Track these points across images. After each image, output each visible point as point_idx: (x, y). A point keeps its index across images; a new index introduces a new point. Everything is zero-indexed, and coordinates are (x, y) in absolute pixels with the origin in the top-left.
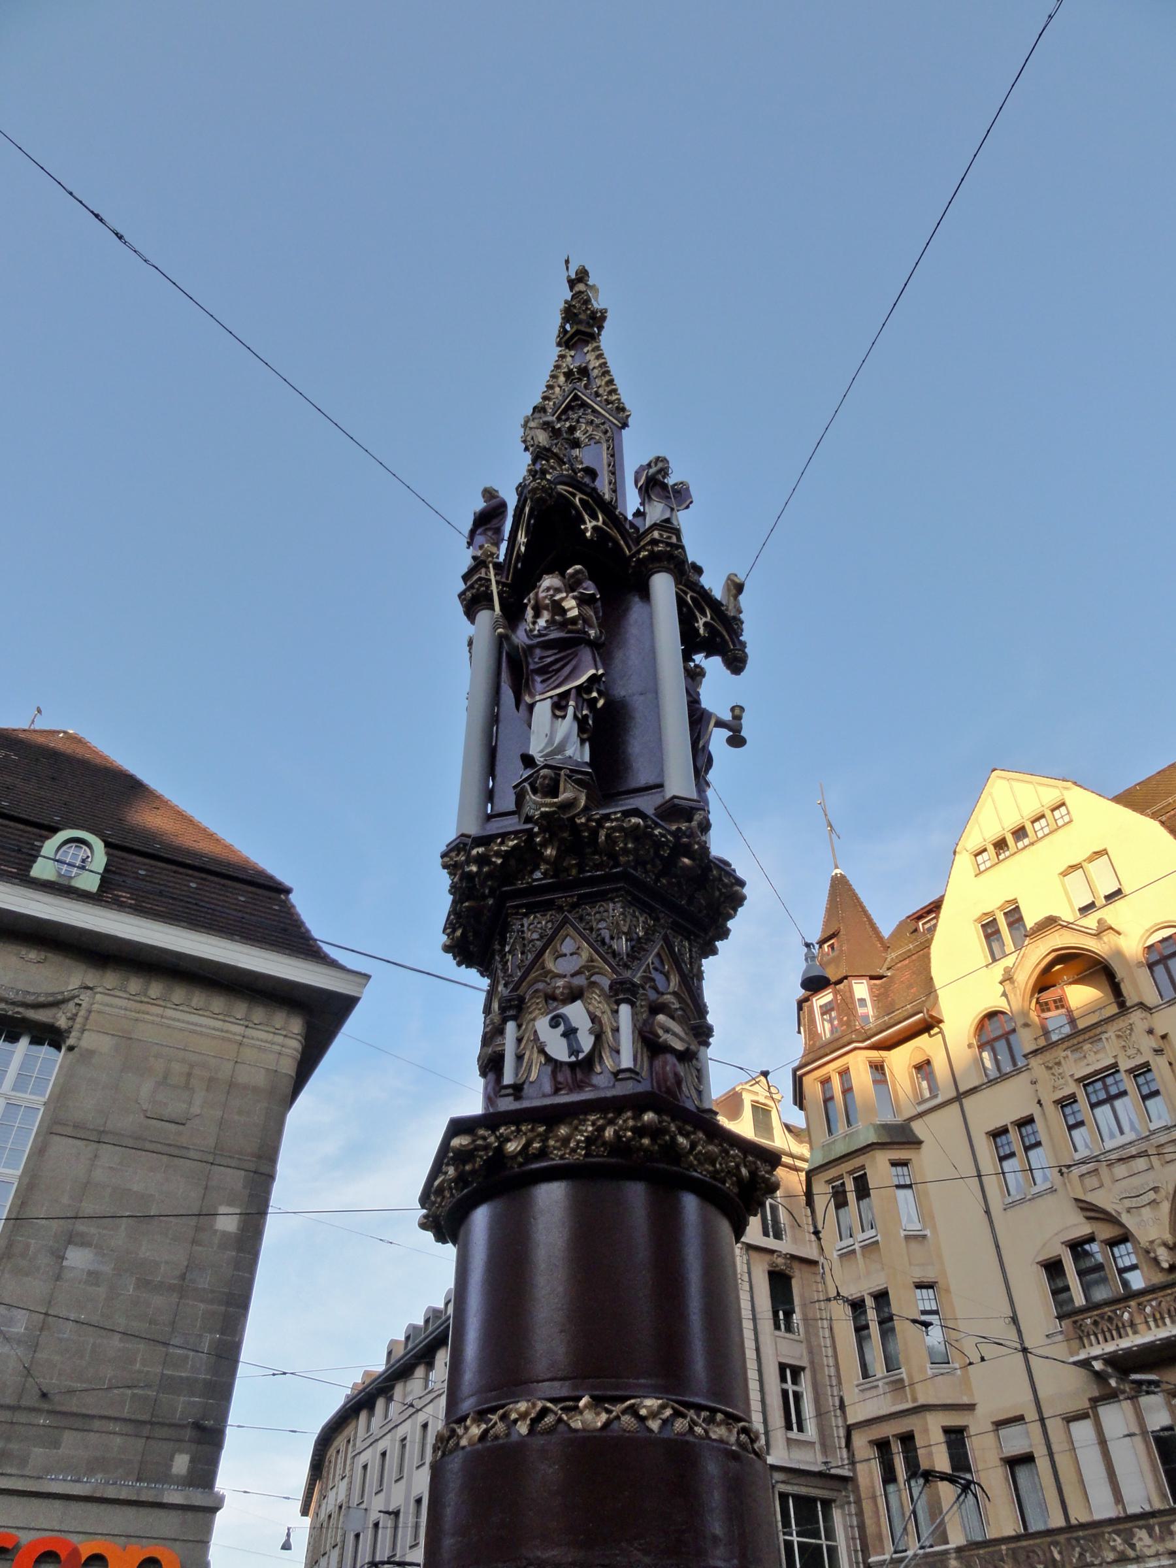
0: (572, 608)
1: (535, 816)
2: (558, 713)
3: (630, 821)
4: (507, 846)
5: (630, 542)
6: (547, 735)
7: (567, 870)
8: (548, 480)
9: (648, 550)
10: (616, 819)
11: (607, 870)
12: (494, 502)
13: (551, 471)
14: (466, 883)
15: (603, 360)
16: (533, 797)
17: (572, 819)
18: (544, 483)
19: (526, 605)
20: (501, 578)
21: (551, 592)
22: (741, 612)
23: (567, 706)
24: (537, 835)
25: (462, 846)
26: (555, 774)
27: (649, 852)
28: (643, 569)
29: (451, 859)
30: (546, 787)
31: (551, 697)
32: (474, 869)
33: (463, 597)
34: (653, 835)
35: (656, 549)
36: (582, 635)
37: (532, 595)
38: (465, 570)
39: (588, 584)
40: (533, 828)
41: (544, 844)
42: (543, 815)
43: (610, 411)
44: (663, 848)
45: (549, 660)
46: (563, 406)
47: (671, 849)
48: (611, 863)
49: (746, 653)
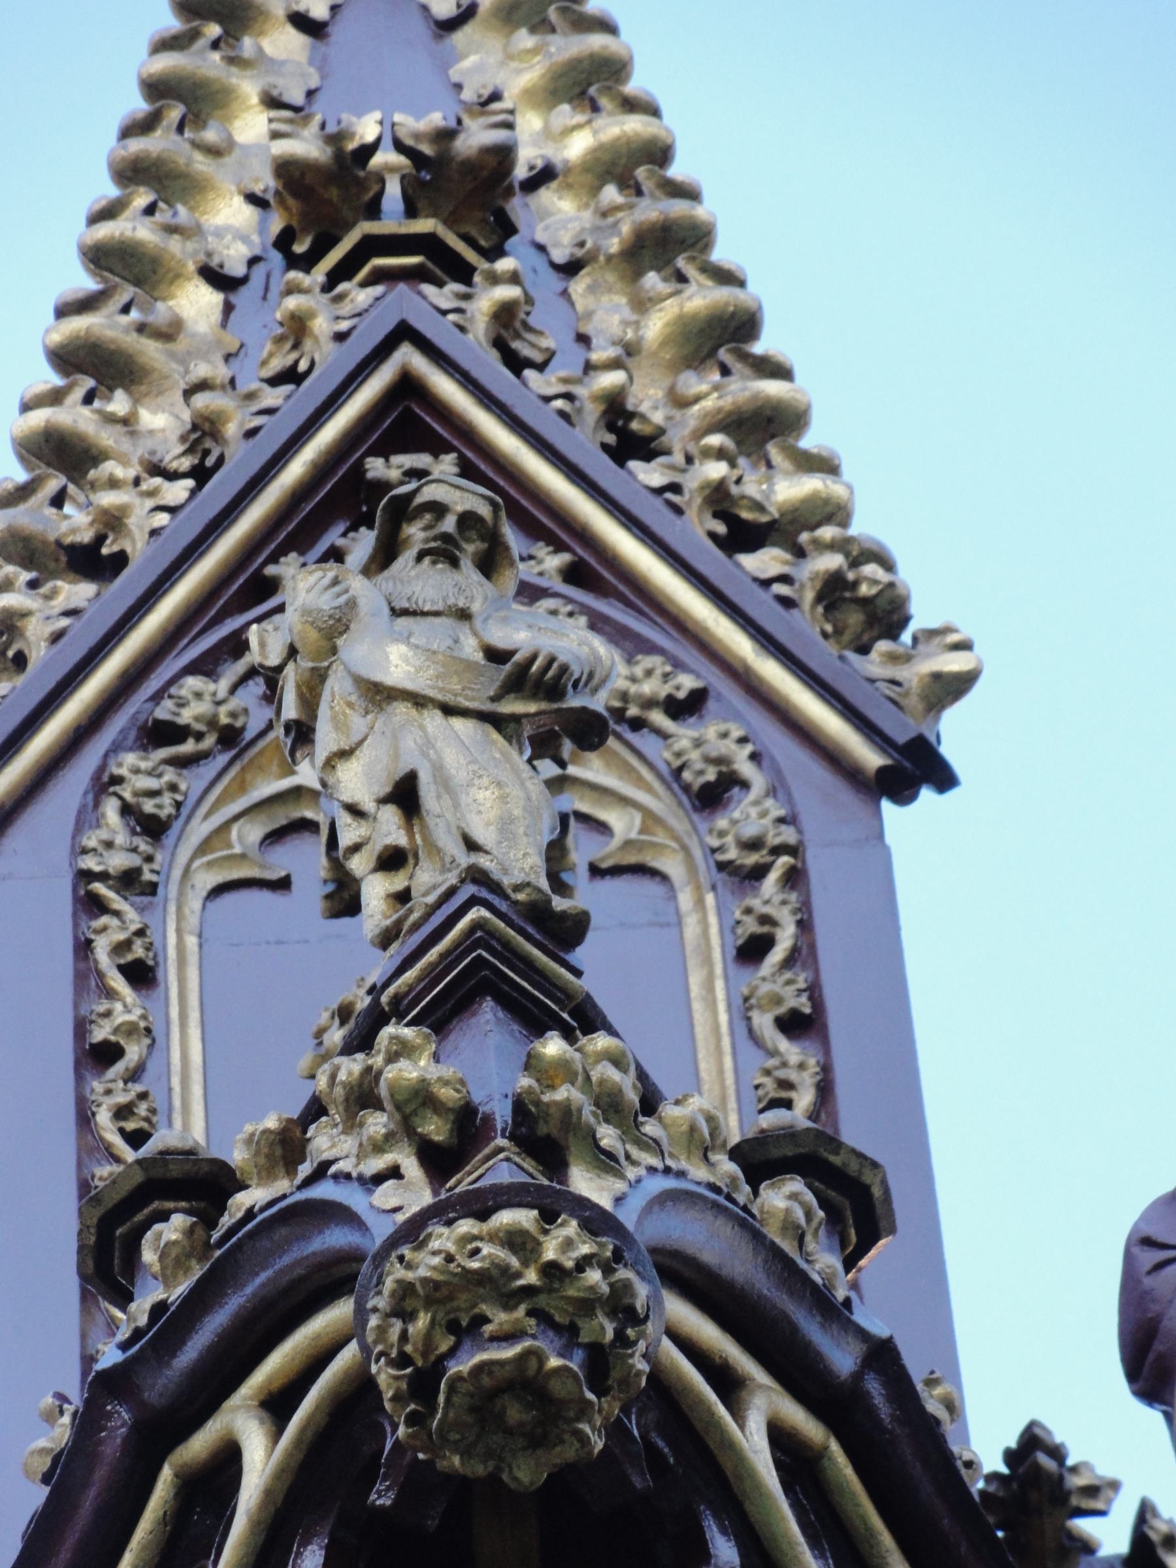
13: (608, 1136)
15: (634, 125)
43: (762, 607)
46: (296, 469)
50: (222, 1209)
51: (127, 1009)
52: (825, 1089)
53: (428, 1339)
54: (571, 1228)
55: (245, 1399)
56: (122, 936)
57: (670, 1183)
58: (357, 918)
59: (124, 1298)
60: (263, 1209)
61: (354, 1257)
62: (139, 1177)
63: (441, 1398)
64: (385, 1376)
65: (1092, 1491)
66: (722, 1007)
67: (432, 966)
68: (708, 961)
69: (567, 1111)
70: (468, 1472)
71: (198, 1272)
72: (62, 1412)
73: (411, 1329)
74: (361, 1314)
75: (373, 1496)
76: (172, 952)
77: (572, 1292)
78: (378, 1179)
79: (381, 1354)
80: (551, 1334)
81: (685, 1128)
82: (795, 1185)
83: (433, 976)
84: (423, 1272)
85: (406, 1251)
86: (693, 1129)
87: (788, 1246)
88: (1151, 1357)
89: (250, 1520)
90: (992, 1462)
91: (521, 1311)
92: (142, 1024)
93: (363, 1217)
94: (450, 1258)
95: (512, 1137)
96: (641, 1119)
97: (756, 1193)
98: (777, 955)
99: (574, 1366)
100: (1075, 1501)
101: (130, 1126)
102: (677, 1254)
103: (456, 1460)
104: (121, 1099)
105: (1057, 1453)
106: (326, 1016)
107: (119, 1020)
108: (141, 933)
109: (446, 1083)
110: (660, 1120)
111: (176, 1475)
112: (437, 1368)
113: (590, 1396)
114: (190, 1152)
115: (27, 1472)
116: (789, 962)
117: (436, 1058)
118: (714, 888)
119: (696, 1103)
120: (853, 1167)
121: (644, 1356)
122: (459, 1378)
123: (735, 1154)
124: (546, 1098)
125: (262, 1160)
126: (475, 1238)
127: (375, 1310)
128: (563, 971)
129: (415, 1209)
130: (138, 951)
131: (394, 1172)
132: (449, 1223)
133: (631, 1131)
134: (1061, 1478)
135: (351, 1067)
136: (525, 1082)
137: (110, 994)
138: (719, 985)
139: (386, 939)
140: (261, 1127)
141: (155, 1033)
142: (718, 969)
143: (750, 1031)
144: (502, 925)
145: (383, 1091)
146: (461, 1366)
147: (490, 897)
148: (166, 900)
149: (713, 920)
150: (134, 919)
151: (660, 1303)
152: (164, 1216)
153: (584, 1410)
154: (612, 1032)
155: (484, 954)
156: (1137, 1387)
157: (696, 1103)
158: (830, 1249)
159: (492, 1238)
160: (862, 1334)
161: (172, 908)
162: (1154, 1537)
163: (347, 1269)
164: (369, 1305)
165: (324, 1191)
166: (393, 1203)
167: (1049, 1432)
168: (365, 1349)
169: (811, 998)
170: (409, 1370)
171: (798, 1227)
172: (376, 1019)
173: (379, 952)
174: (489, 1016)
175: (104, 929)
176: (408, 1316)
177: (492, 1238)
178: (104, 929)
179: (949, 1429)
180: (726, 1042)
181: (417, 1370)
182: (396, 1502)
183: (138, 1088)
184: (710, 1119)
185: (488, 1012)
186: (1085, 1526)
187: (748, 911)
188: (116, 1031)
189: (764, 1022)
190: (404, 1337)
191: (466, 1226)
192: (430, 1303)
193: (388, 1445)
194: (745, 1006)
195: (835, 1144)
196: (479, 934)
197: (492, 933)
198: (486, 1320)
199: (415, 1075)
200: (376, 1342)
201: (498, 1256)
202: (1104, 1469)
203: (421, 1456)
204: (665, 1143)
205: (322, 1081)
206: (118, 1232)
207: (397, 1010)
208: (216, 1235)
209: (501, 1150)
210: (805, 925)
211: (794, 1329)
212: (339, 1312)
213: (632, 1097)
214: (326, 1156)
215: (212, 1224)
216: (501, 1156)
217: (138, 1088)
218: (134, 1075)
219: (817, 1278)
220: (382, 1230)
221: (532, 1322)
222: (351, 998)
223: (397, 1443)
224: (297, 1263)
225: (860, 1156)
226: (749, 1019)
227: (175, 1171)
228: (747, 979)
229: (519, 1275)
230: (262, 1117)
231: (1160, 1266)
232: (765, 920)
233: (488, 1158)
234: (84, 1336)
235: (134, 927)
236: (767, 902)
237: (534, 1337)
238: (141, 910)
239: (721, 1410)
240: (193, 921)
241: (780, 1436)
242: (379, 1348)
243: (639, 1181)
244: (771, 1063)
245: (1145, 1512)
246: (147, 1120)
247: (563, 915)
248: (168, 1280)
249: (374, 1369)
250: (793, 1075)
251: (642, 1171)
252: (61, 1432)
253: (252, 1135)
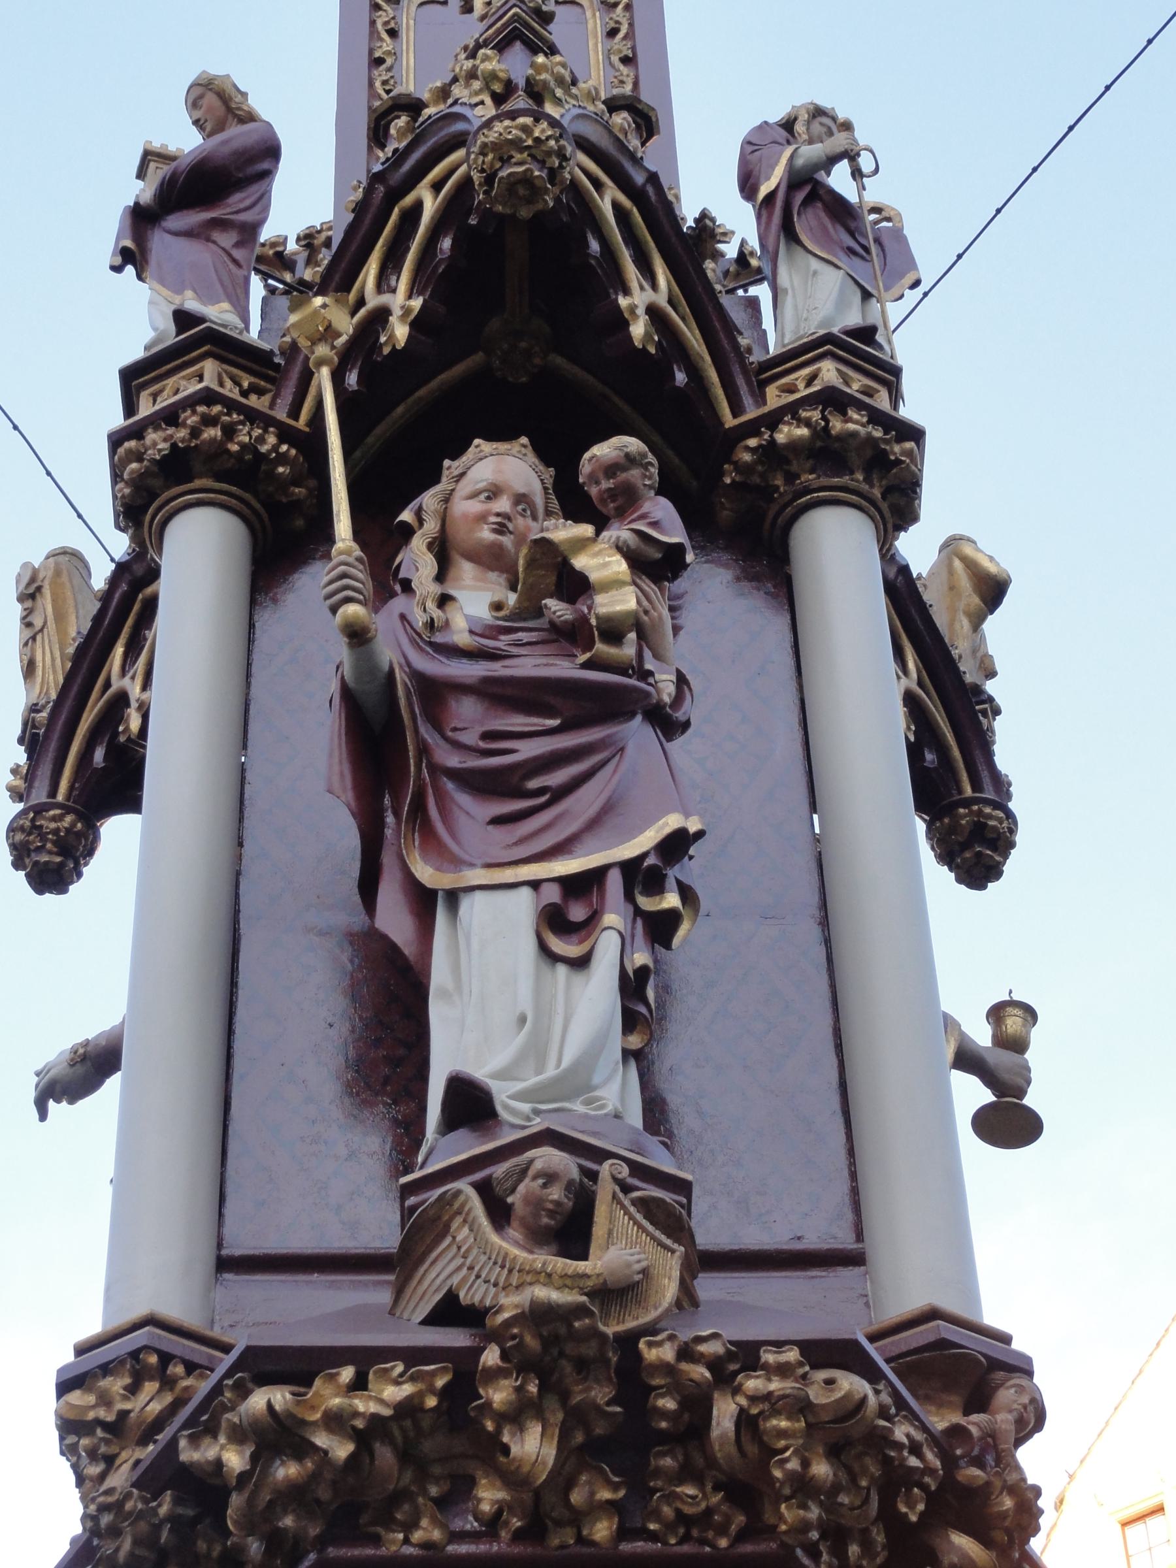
0: (614, 584)
1: (500, 1309)
2: (558, 945)
3: (830, 1382)
4: (381, 1401)
5: (740, 381)
6: (522, 1020)
7: (577, 1518)
8: (554, 123)
9: (807, 423)
10: (783, 1370)
11: (723, 1543)
12: (237, 135)
13: (559, 92)
14: (177, 1501)
16: (494, 1238)
17: (628, 1341)
18: (542, 130)
19: (407, 532)
20: (272, 405)
21: (503, 504)
22: (991, 674)
23: (591, 922)
24: (493, 1375)
25: (153, 1359)
26: (584, 1171)
27: (866, 1501)
28: (779, 482)
29: (105, 1400)
30: (551, 1214)
31: (535, 885)
32: (235, 1460)
33: (131, 444)
34: (883, 1440)
35: (837, 425)
36: (632, 682)
37: (429, 499)
38: (135, 353)
39: (662, 509)
40: (477, 1352)
41: (516, 1416)
42: (539, 1315)
44: (909, 1490)
45: (527, 750)
47: (932, 1498)
48: (740, 1519)
49: (1010, 815)
50: (419, 115)
51: (388, 46)
52: (636, 84)
53: (492, 164)
54: (544, 125)
55: (426, 184)
56: (387, 19)
57: (580, 111)
58: (472, 15)
59: (382, 146)
60: (435, 115)
61: (465, 134)
62: (390, 103)
63: (496, 185)
64: (476, 176)
65: (725, 234)
66: (600, 53)
67: (498, 29)
68: (596, 37)
69: (545, 82)
70: (504, 212)
71: (410, 138)
72: (359, 187)
73: (486, 160)
74: (468, 154)
75: (470, 221)
76: (404, 25)
77: (544, 148)
78: (476, 105)
79: (475, 168)
80: (536, 163)
81: (586, 92)
82: (625, 114)
83: (499, 32)
84: (491, 139)
85: (485, 131)
86: (589, 92)
87: (621, 137)
88: (748, 185)
89: (426, 227)
90: (690, 222)
91: (526, 154)
92: (393, 51)
93: (471, 119)
94: (501, 134)
95: (525, 92)
96: (571, 87)
97: (611, 116)
98: (621, 35)
99: (544, 175)
100: (718, 238)
101: (387, 88)
102: (580, 137)
103: (500, 208)
104: (385, 78)
105: (713, 220)
106: (459, 50)
107: (385, 49)
108: (393, 18)
109: (502, 71)
110: (578, 88)
111: (400, 211)
112: (495, 174)
113: (549, 186)
114: (409, 95)
115: (347, 209)
116: (625, 38)
117: (499, 61)
118: (599, 10)
119: (591, 83)
120: (646, 110)
121: (569, 173)
122: (502, 178)
123: (604, 102)
124: (538, 78)
125: (435, 98)
126: (510, 127)
127: (473, 152)
128: (545, 33)
129: (489, 116)
130: (392, 25)
131: (482, 103)
132: (501, 121)
133: (567, 92)
134: (714, 229)
135: (468, 64)
136: (530, 71)
137: (382, 40)
138: (600, 45)
139: (483, 18)
140: (435, 86)
141: (397, 54)
142: (600, 40)
143: (610, 63)
144: (524, 14)
145: (479, 73)
146: (503, 173)
147: (521, 5)
148: (403, 7)
149: (598, 22)
150: (391, 13)
151: (575, 155)
152: (398, 117)
153: (546, 191)
154: (561, 55)
155: (518, 25)
156: (744, 194)
157: (591, 83)
158: (637, 138)
159: (516, 127)
160: (647, 170)
161: (405, 10)
162: (746, 252)
163: (462, 138)
164: (472, 150)
165: (457, 109)
166: (481, 113)
167: (710, 213)
168: (469, 167)
169: (632, 51)
170: (485, 175)
171: (625, 129)
172: (478, 46)
173: (479, 23)
174: (518, 48)
175: (380, 16)
176: (485, 155)
177: (516, 127)
178: (380, 16)
179: (676, 206)
180: (601, 66)
181: (488, 174)
182: (478, 222)
183: (391, 74)
184: (596, 89)
185: (518, 46)
186: (721, 246)
187: (611, 19)
188: (383, 53)
189: (615, 59)
190: (483, 162)
191: (507, 123)
192: (493, 150)
193: (476, 203)
194: (608, 54)
195: (640, 101)
196: (516, 18)
197: (520, 17)
198: (512, 157)
199: (491, 67)
200: (473, 164)
201: (420, 855)
202: (729, 227)
203: (488, 206)
204: (579, 96)
205: (457, 70)
206: (382, 123)
207: (485, 44)
208: (417, 124)
209: (520, 96)
210: (631, 25)
211: (622, 167)
212: (460, 154)
213: (568, 79)
214: (458, 96)
215: (415, 120)
216: (521, 98)
217: (391, 74)
218: (389, 69)
219: (632, 149)
220: (477, 123)
221: (529, 158)
222: (468, 43)
223: (480, 202)
224: (446, 135)
225: (648, 105)
226: (610, 58)
227: (403, 101)
228: (610, 43)
229: (525, 141)
230: (435, 81)
231: (753, 152)
232: (617, 22)
233: (516, 99)
234: (368, 163)
235: (391, 16)
236: (618, 16)
237: (530, 164)
238: (394, 10)
239: (595, 194)
240: (412, 14)
241: (616, 206)
242: (474, 166)
243: (569, 109)
244: (617, 74)
245: (743, 243)
246: (393, 86)
247: (546, 12)
248: (400, 141)
249: (472, 174)
250: (625, 79)
251: (571, 106)
252: (359, 194)
253: (432, 88)
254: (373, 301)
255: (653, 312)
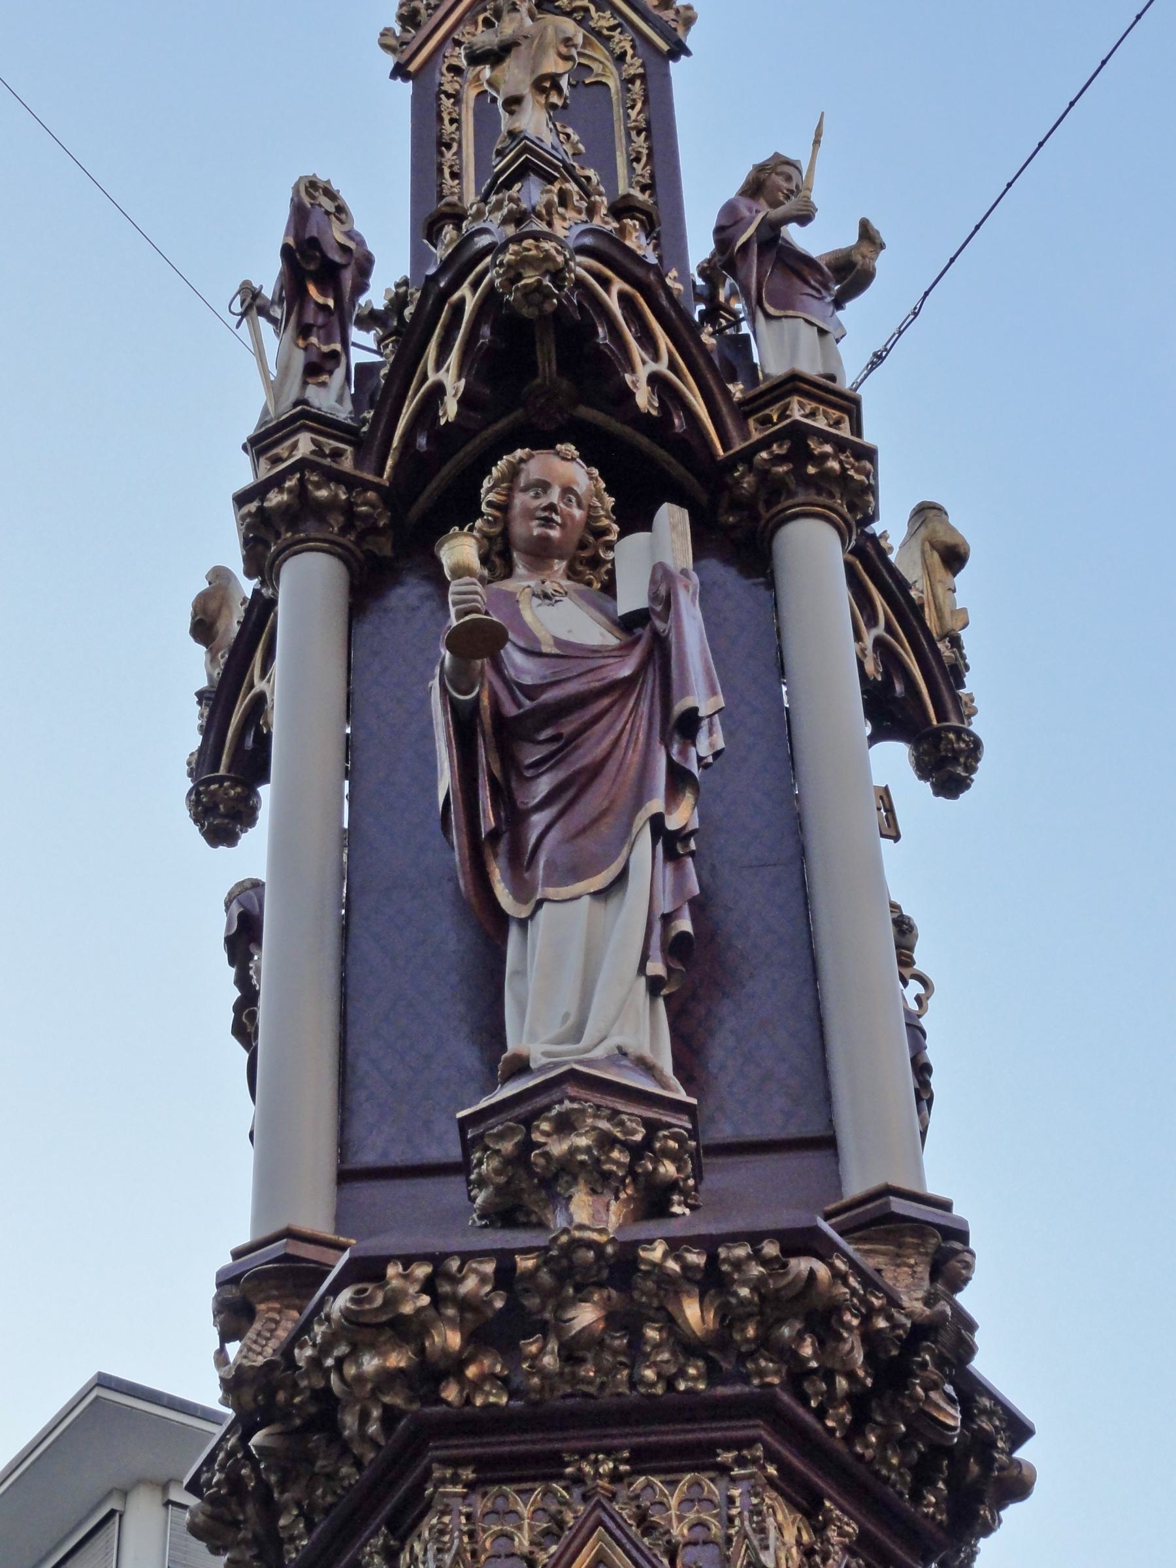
185: (533, 177)
241: (623, 297)
254: (432, 377)
255: (655, 380)
